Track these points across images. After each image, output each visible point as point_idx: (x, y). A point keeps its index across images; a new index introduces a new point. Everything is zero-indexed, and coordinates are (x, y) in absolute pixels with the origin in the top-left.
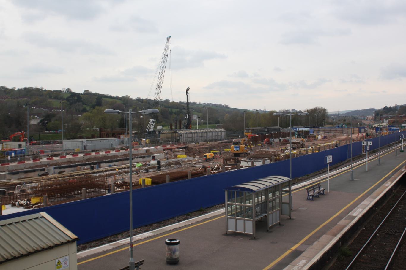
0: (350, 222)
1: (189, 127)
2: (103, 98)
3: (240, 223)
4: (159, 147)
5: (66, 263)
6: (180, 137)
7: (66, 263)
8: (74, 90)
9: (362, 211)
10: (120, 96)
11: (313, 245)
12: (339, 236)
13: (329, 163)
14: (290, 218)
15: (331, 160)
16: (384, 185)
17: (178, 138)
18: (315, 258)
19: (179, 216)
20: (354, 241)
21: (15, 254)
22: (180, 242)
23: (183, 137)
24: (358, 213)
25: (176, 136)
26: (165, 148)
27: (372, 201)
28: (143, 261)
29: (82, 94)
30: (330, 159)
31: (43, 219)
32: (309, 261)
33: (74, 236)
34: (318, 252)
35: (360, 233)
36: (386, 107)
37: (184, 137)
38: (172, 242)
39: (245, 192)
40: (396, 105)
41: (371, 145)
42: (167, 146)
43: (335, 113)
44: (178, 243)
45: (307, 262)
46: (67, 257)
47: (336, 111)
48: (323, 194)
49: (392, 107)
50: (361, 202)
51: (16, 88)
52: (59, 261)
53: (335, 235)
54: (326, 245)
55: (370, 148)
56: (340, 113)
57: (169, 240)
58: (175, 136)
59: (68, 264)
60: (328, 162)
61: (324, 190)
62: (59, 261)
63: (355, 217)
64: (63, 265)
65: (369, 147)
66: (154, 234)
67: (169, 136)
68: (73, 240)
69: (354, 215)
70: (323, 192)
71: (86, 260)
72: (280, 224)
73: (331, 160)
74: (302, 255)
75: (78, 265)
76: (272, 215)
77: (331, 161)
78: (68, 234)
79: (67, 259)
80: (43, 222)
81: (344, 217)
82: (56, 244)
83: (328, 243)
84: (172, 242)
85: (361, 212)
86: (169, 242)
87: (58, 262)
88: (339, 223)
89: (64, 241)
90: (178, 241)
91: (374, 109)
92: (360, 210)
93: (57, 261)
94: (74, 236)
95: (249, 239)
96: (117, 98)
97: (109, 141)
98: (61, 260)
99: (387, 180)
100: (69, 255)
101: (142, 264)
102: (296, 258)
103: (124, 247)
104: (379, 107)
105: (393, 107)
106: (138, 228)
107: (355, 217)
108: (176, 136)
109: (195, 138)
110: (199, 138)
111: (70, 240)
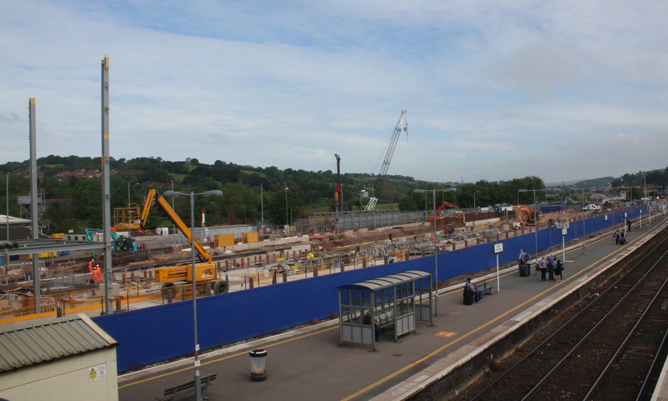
0: (508, 329)
1: (635, 198)
2: (241, 171)
3: (357, 330)
4: (304, 236)
5: (102, 373)
6: (336, 222)
7: (102, 373)
8: (202, 161)
9: (531, 314)
10: (264, 168)
11: (446, 358)
12: (486, 346)
13: (497, 253)
14: (432, 325)
15: (501, 249)
16: (577, 280)
17: (333, 223)
18: (440, 373)
19: (302, 325)
20: (513, 353)
21: (35, 360)
22: (268, 353)
23: (339, 221)
24: (523, 319)
25: (332, 221)
26: (313, 237)
27: (550, 301)
28: (215, 375)
29: (212, 166)
30: (499, 248)
31: (80, 322)
32: (431, 376)
33: (110, 340)
34: (447, 367)
35: (526, 343)
36: (627, 174)
37: (342, 222)
38: (257, 353)
39: (362, 292)
40: (640, 171)
41: (568, 227)
42: (315, 235)
43: (559, 184)
44: (265, 354)
45: (428, 378)
46: (104, 365)
47: (560, 181)
48: (490, 294)
49: (635, 174)
50: (534, 304)
51: (125, 160)
52: (93, 370)
53: (480, 345)
54: (462, 357)
55: (567, 232)
56: (565, 184)
57: (253, 351)
58: (329, 221)
59: (105, 373)
60: (496, 252)
61: (491, 288)
62: (93, 370)
63: (518, 322)
64: (98, 374)
65: (566, 231)
66: (250, 346)
67: (321, 221)
68: (111, 347)
69: (518, 320)
70: (490, 292)
71: (156, 376)
72: (415, 333)
73: (501, 249)
74: (426, 369)
75: (118, 378)
76: (402, 321)
77: (502, 250)
78: (105, 339)
79: (103, 368)
80: (79, 325)
81: (502, 323)
82: (89, 350)
83: (466, 354)
84: (257, 353)
85: (529, 316)
86: (253, 353)
87: (92, 371)
88: (491, 331)
89: (99, 346)
90: (265, 352)
91: (610, 178)
92: (530, 312)
93: (90, 369)
94: (114, 342)
95: (368, 352)
96: (260, 170)
97: (216, 231)
98: (95, 368)
99: (584, 274)
100: (106, 363)
101: (215, 379)
102: (416, 373)
103: (208, 361)
104: (618, 174)
105: (636, 174)
106: (243, 340)
107: (518, 322)
108: (332, 221)
109: (356, 224)
110: (361, 223)
111: (107, 345)
